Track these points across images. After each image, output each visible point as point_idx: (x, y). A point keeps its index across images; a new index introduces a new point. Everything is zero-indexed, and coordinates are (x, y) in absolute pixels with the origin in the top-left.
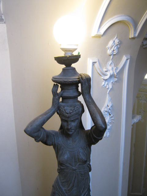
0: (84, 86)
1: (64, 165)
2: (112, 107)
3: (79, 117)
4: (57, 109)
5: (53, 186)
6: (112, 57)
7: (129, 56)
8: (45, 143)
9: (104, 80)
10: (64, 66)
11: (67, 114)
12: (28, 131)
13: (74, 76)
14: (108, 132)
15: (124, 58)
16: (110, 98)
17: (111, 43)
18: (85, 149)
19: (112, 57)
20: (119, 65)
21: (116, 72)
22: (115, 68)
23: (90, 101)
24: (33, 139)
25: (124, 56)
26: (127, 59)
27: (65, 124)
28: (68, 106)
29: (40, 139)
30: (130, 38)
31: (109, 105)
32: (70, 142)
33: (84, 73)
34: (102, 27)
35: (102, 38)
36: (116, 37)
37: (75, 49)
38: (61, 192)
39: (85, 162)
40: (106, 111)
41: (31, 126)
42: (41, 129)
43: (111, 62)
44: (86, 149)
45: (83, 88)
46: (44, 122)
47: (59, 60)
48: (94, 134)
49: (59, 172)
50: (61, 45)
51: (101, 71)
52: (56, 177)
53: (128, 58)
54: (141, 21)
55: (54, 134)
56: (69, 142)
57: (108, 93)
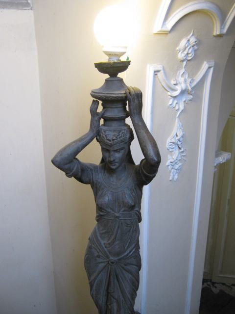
0: (132, 103)
1: (104, 209)
2: (182, 137)
3: (126, 146)
4: (96, 133)
5: (89, 239)
6: (185, 63)
7: (213, 63)
8: (80, 180)
9: (171, 98)
10: (107, 76)
11: (108, 142)
12: (57, 161)
13: (120, 89)
14: (176, 173)
15: (205, 66)
16: (181, 124)
17: (183, 43)
18: (133, 190)
19: (185, 63)
20: (197, 75)
21: (190, 86)
22: (190, 80)
23: (140, 124)
24: (64, 173)
25: (205, 62)
26: (210, 68)
27: (107, 154)
28: (110, 131)
29: (73, 174)
30: (214, 36)
31: (178, 134)
32: (113, 179)
33: (133, 86)
34: (169, 19)
35: (169, 35)
36: (192, 34)
37: (123, 53)
38: (99, 247)
39: (133, 207)
40: (174, 143)
41: (61, 155)
42: (74, 160)
43: (183, 70)
44: (135, 190)
45: (131, 107)
46: (78, 151)
47: (102, 68)
48: (144, 170)
49: (97, 221)
50: (103, 46)
51: (167, 84)
52: (95, 226)
53: (210, 66)
54: (231, 11)
55: (94, 168)
56: (112, 180)
57: (177, 116)
